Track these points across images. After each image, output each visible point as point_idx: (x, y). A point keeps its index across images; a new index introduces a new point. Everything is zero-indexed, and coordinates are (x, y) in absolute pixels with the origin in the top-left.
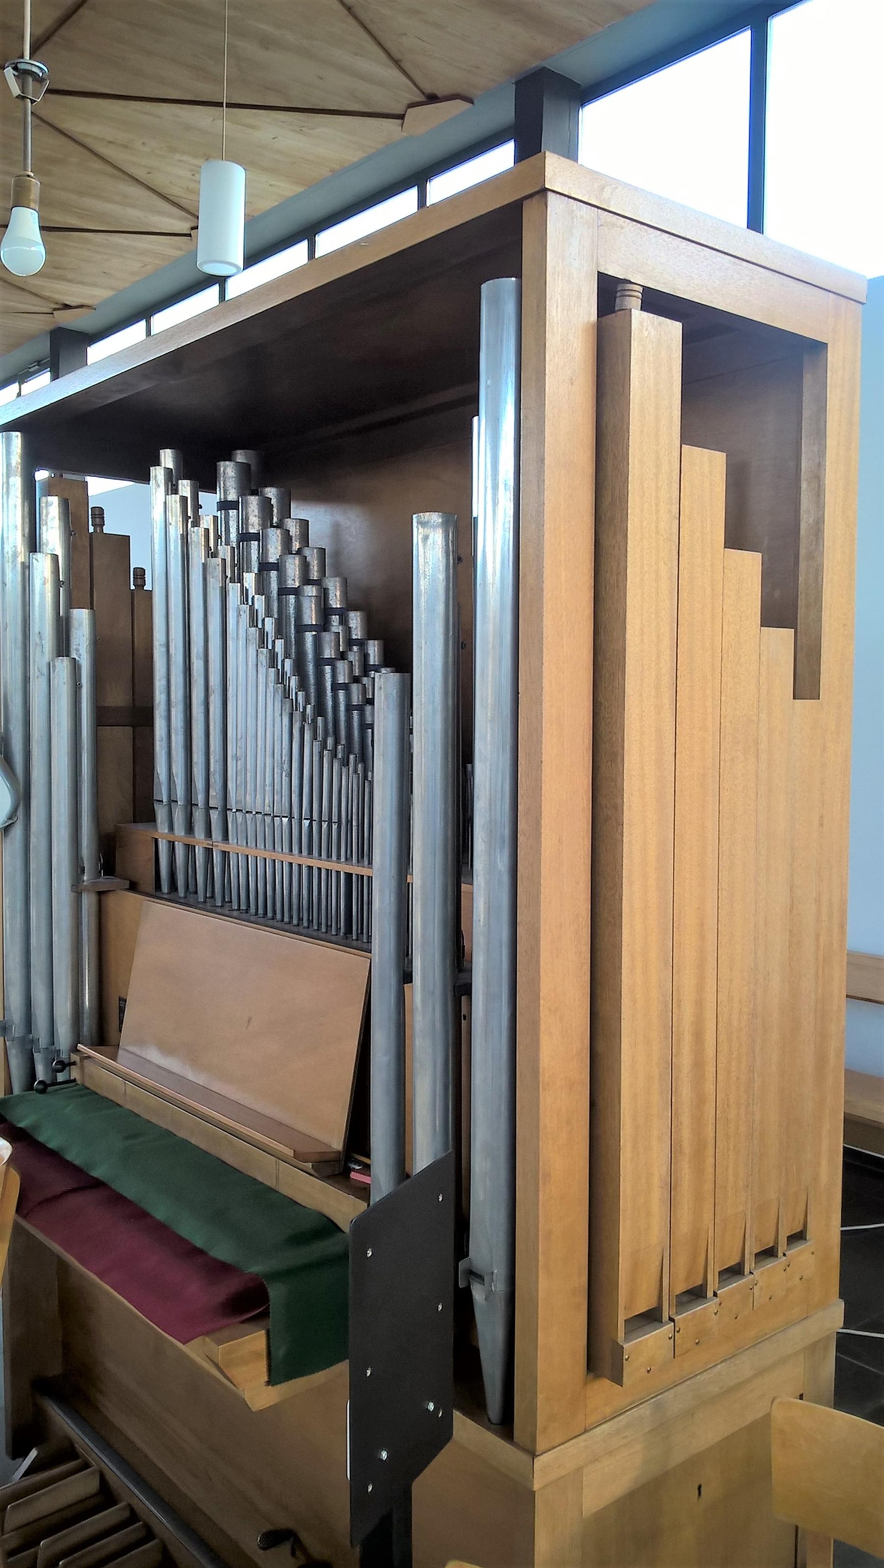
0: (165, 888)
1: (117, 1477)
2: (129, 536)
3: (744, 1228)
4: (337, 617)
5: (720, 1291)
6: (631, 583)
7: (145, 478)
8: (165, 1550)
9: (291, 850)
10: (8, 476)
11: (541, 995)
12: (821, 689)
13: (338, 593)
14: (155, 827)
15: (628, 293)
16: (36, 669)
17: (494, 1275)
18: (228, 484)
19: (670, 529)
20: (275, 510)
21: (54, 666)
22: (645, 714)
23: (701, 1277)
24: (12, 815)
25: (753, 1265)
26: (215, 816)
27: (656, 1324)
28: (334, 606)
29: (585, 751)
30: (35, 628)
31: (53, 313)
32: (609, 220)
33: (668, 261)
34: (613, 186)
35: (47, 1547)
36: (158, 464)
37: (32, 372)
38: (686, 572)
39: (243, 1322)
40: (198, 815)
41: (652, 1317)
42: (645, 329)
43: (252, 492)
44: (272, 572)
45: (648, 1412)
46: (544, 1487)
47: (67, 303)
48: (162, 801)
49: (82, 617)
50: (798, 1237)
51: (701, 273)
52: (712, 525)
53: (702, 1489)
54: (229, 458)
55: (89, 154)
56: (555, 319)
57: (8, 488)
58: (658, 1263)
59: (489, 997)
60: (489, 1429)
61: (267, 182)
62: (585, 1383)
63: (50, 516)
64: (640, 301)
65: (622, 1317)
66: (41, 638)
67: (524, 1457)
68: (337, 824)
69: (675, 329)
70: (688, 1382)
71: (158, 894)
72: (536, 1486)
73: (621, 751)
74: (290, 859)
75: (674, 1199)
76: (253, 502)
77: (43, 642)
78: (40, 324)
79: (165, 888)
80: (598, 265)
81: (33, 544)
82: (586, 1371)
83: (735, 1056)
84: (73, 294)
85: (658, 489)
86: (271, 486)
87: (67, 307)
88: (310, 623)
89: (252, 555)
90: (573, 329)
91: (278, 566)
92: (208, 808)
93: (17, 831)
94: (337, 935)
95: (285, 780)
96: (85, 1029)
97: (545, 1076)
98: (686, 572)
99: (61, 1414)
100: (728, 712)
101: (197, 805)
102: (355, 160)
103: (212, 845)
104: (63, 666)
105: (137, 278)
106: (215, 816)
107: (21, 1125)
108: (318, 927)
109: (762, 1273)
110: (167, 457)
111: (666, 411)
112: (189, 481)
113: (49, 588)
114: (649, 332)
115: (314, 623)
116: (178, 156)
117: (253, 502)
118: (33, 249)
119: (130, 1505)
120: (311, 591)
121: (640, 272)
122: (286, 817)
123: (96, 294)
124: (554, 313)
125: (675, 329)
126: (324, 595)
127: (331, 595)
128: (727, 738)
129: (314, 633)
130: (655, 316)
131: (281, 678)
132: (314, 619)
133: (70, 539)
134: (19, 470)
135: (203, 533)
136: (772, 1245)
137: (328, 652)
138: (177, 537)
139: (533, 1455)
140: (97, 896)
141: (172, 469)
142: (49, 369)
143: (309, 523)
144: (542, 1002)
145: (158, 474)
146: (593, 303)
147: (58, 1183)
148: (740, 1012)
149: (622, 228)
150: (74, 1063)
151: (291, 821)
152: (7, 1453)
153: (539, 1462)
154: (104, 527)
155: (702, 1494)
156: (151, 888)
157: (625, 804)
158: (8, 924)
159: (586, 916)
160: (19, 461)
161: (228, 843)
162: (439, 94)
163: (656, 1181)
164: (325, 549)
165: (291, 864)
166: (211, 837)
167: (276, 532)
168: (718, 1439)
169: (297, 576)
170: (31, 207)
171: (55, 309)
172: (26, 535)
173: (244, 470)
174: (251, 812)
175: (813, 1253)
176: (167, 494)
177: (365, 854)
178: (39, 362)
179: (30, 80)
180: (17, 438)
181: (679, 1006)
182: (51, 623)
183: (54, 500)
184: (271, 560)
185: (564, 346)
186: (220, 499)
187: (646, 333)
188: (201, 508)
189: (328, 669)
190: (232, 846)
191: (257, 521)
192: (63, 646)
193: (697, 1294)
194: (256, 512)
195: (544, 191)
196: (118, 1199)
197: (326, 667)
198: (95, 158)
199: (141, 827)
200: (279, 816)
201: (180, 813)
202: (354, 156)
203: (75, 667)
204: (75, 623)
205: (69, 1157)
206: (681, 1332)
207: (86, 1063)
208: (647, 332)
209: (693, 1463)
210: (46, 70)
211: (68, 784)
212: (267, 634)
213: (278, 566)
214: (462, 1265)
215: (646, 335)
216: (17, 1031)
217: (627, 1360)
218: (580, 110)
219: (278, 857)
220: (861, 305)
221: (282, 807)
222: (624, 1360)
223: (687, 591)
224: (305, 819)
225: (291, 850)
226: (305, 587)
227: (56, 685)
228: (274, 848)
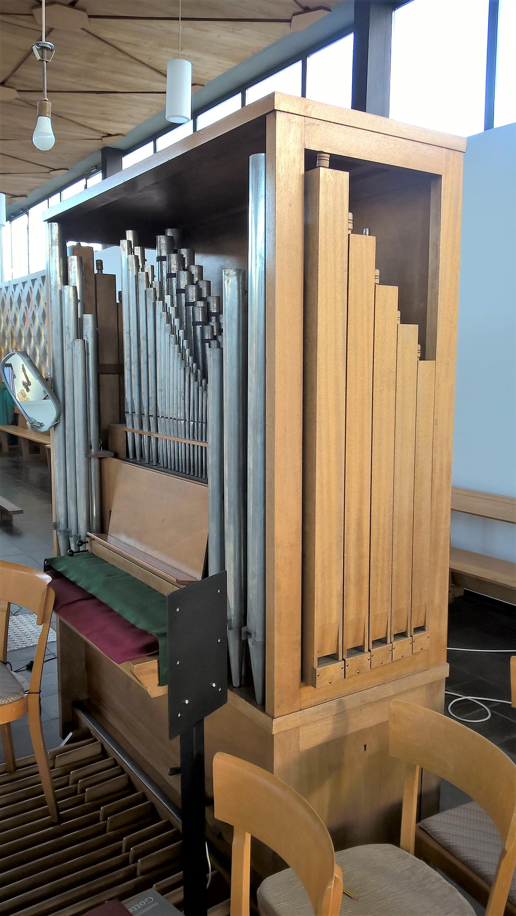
0: (131, 457)
1: (110, 746)
2: (115, 275)
3: (387, 621)
4: (215, 317)
5: (372, 650)
6: (320, 304)
7: (118, 244)
8: (129, 778)
9: (198, 439)
10: (52, 246)
11: (276, 502)
12: (437, 355)
13: (215, 305)
14: (126, 426)
15: (321, 158)
16: (67, 346)
17: (257, 634)
18: (161, 248)
19: (343, 276)
20: (186, 261)
21: (74, 344)
22: (328, 368)
23: (362, 642)
24: (57, 419)
25: (393, 639)
26: (152, 419)
27: (336, 661)
28: (213, 312)
29: (299, 387)
30: (65, 325)
31: (102, 139)
32: (311, 122)
33: (346, 140)
34: (313, 105)
35: (74, 774)
36: (125, 238)
37: (93, 172)
38: (352, 297)
39: (148, 656)
40: (145, 420)
41: (333, 658)
42: (327, 177)
43: (174, 251)
44: (182, 294)
45: (335, 705)
46: (279, 733)
47: (109, 133)
48: (129, 412)
49: (88, 318)
50: (420, 629)
51: (365, 144)
52: (367, 273)
53: (367, 747)
54: (164, 233)
55: (115, 50)
56: (281, 175)
57: (52, 252)
58: (336, 632)
59: (255, 504)
60: (256, 707)
61: (216, 61)
62: (300, 687)
63: (73, 266)
64: (329, 162)
65: (316, 656)
66: (68, 330)
67: (269, 719)
68: (201, 423)
69: (345, 176)
70: (357, 693)
71: (128, 459)
72: (274, 732)
73: (315, 386)
74: (184, 441)
75: (346, 602)
76: (174, 257)
77: (70, 331)
78: (97, 145)
79: (131, 457)
80: (305, 145)
81: (66, 281)
82: (300, 681)
83: (382, 536)
84: (112, 128)
85: (335, 257)
86: (184, 248)
87: (109, 135)
88: (199, 321)
89: (173, 285)
90: (291, 178)
91: (184, 291)
92: (149, 416)
93: (60, 427)
94: (189, 474)
95: (182, 401)
96: (94, 526)
97: (277, 541)
98: (352, 297)
99: (85, 716)
100: (378, 367)
101: (144, 414)
102: (266, 46)
103: (150, 435)
104: (79, 343)
105: (148, 118)
106: (152, 419)
107: (59, 570)
108: (194, 474)
109: (398, 644)
110: (130, 235)
111: (340, 217)
112: (140, 247)
113: (72, 303)
114: (330, 178)
115: (201, 321)
116: (165, 49)
117: (174, 257)
118: (48, 137)
119: (114, 759)
120: (200, 304)
121: (329, 147)
122: (183, 420)
123: (125, 128)
124: (280, 170)
125: (345, 176)
126: (207, 305)
127: (211, 305)
128: (377, 380)
129: (201, 326)
130: (333, 170)
131: (181, 351)
132: (201, 319)
133: (83, 277)
134: (57, 242)
135: (145, 275)
136: (405, 631)
137: (207, 337)
138: (133, 276)
139: (273, 718)
140: (99, 460)
141: (131, 241)
142: (101, 171)
143: (203, 267)
144: (275, 506)
145: (124, 243)
146: (302, 165)
147: (73, 595)
148: (385, 516)
149: (318, 125)
150: (87, 542)
151: (185, 422)
152: (60, 736)
153: (275, 722)
154: (103, 270)
155: (367, 749)
156: (124, 456)
157: (317, 412)
158: (57, 474)
159: (299, 466)
160: (57, 238)
161: (158, 434)
162: (311, 7)
163: (334, 592)
164: (210, 281)
165: (185, 444)
166: (150, 430)
167: (184, 273)
168: (375, 724)
169: (194, 296)
170: (47, 116)
171: (104, 137)
172: (61, 276)
173: (170, 241)
174: (168, 418)
175: (429, 637)
176: (129, 254)
177: (204, 437)
178: (96, 167)
179: (45, 50)
180: (55, 226)
181: (349, 511)
182: (73, 322)
183: (75, 258)
184: (182, 288)
185: (285, 187)
186: (158, 255)
187: (328, 179)
188: (146, 261)
189: (207, 344)
190: (161, 435)
191: (176, 267)
192: (79, 334)
193: (359, 649)
194: (175, 262)
195: (274, 111)
196: (101, 604)
197: (207, 344)
198: (119, 52)
199: (119, 426)
200: (180, 420)
201: (137, 418)
202: (264, 44)
203: (85, 345)
204: (85, 322)
205: (79, 584)
206: (349, 666)
207: (93, 542)
208: (329, 179)
209: (363, 733)
210: (53, 45)
211: (82, 404)
212: (176, 327)
213: (184, 291)
214: (244, 629)
215: (328, 180)
216: (62, 527)
217: (318, 676)
218: (393, 12)
219: (180, 440)
220: (463, 153)
221: (181, 415)
222: (317, 676)
223: (353, 307)
224: (191, 421)
225: (198, 439)
226: (197, 302)
227: (75, 354)
228: (185, 437)
